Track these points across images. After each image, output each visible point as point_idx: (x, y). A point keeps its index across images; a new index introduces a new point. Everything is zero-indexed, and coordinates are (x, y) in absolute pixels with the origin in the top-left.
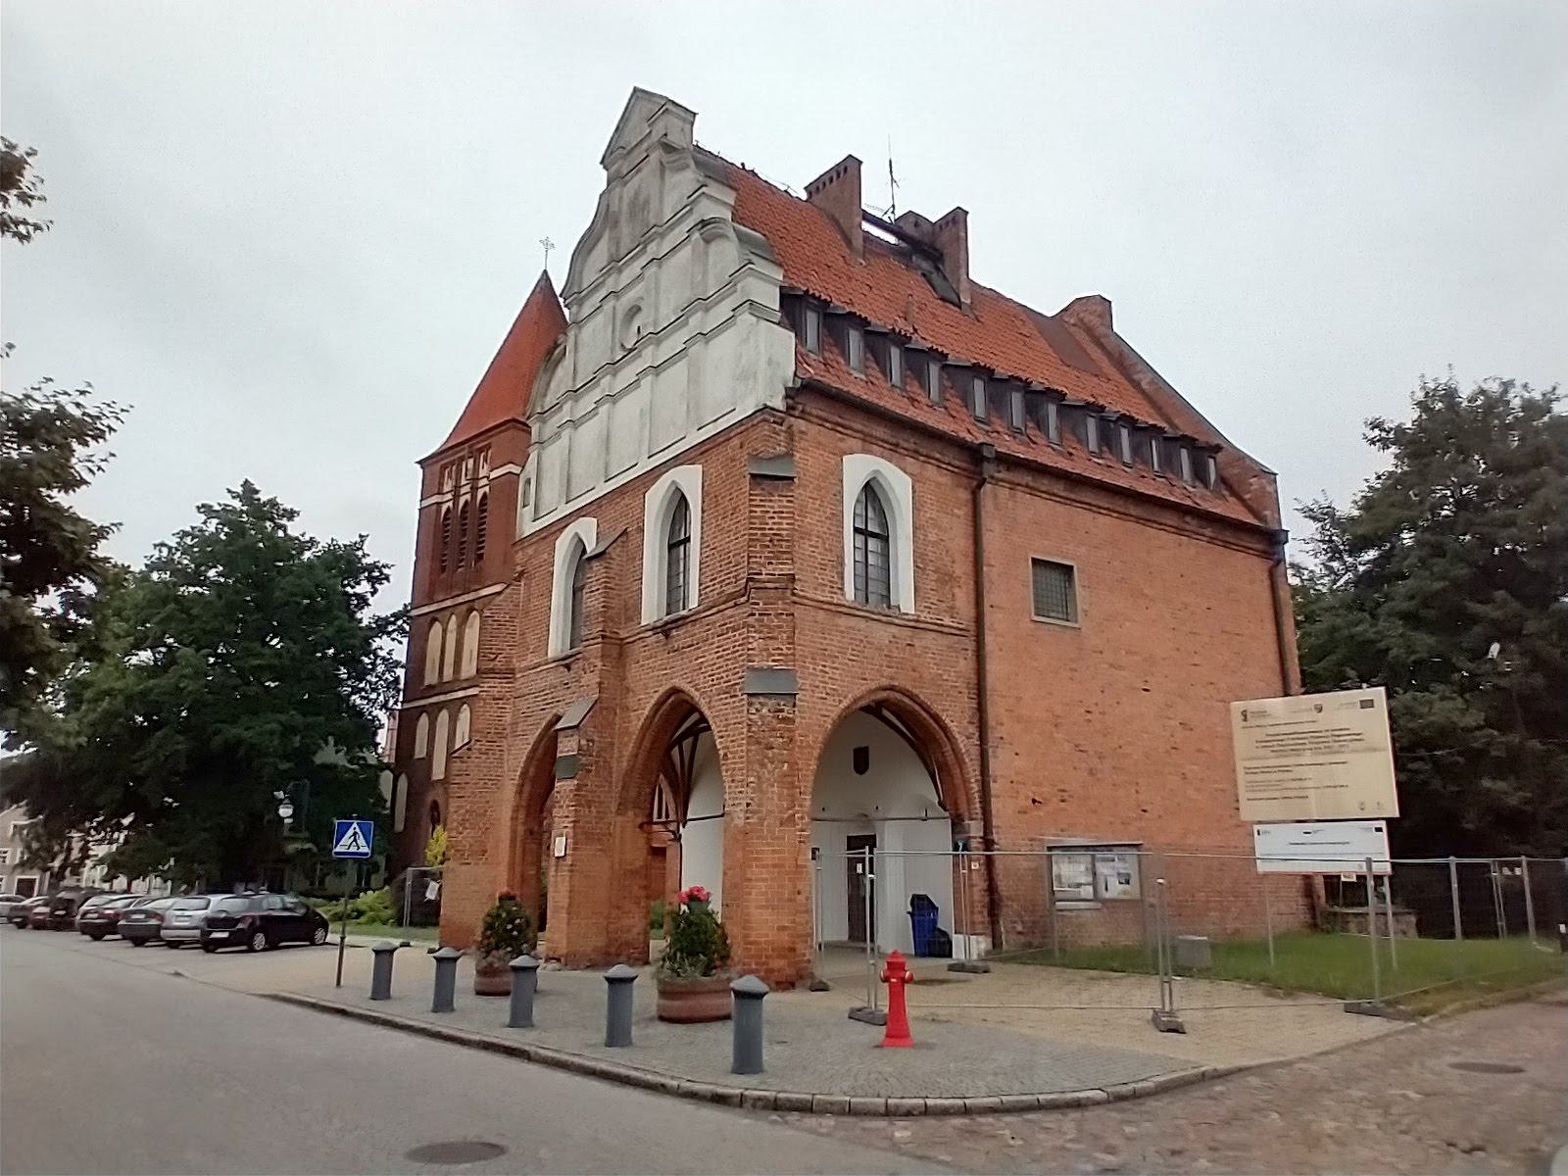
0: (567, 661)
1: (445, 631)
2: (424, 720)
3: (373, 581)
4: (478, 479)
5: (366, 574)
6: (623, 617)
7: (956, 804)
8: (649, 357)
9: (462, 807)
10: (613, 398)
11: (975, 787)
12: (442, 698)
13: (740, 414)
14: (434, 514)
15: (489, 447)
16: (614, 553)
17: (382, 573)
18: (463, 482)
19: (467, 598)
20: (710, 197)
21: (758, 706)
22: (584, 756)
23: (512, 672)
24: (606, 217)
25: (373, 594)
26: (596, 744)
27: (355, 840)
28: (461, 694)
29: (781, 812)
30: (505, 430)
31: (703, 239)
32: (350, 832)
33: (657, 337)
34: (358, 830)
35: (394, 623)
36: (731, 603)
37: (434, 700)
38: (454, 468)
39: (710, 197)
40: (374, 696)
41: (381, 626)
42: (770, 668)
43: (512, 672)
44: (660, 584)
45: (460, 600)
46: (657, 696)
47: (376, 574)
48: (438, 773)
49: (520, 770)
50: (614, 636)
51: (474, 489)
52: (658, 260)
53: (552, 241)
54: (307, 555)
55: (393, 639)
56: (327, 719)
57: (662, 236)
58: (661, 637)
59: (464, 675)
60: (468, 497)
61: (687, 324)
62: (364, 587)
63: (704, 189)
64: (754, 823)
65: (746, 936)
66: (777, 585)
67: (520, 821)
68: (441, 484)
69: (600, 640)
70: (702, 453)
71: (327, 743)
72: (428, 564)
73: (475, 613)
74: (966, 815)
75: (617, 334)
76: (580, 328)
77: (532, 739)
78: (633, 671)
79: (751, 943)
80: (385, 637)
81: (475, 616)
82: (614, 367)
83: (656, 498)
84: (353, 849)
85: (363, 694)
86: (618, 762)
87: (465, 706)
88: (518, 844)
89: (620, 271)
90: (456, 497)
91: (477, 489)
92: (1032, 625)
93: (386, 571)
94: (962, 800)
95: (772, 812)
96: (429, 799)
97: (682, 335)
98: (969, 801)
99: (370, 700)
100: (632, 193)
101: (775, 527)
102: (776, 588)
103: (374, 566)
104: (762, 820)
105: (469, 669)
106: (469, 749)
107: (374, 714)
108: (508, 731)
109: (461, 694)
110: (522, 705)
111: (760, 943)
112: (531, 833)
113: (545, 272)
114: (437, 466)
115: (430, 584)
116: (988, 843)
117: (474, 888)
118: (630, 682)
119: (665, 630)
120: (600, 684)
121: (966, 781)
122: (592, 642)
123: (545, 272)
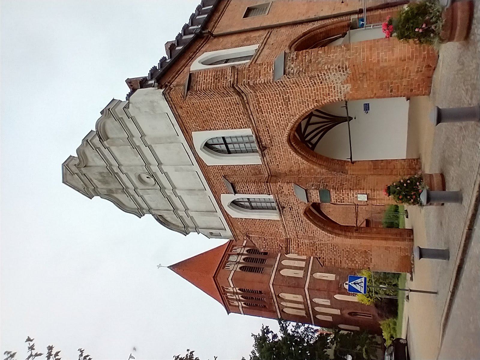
0: (281, 209)
1: (286, 307)
2: (318, 317)
3: (268, 332)
4: (234, 292)
5: (266, 334)
6: (259, 176)
7: (343, 27)
8: (155, 168)
9: (345, 262)
10: (174, 188)
11: (335, 20)
12: (310, 309)
13: (220, 215)
14: (246, 309)
15: (223, 287)
16: (232, 180)
17: (266, 329)
18: (235, 298)
19: (274, 298)
20: (92, 139)
21: (290, 69)
22: (319, 187)
23: (287, 239)
24: (109, 196)
25: (273, 333)
26: (314, 183)
27: (358, 284)
28: (309, 302)
29: (343, 51)
30: (217, 281)
31: (107, 140)
32: (354, 286)
33: (147, 164)
34: (353, 282)
35: (283, 324)
36: (247, 105)
37: (311, 312)
38: (230, 301)
39: (92, 139)
40: (310, 337)
41: (284, 329)
42: (273, 72)
43: (287, 239)
44: (243, 156)
45: (275, 300)
46: (292, 153)
47: (265, 331)
48: (337, 312)
49: (328, 234)
50: (267, 178)
51: (237, 293)
52: (119, 165)
53: (159, 265)
54: (257, 355)
55: (289, 325)
56: (317, 351)
57: (111, 165)
58: (266, 152)
59: (302, 300)
60: (240, 296)
61: (139, 146)
62: (270, 336)
63: (88, 141)
64: (349, 63)
65: (409, 58)
66: (236, 73)
67: (352, 235)
68: (236, 306)
69: (268, 184)
70: (187, 132)
71: (326, 351)
72: (263, 312)
73: (280, 295)
74: (349, 22)
75: (150, 188)
76: (151, 208)
77: (315, 228)
78: (283, 168)
79: (413, 56)
80: (288, 328)
81: (281, 295)
82: (162, 189)
83: (234, 213)
84: (363, 285)
85: (309, 340)
86: (323, 174)
87: (313, 300)
88: (362, 235)
89: (127, 188)
90: (240, 300)
91: (237, 292)
92: (269, 14)
93: (265, 327)
94: (342, 24)
95: (343, 56)
96: (347, 316)
97: (143, 147)
98: (342, 21)
99: (311, 338)
100: (100, 183)
101: (211, 78)
102: (237, 74)
103: (263, 332)
104: (347, 59)
105: (300, 298)
106: (320, 258)
107: (316, 337)
108: (312, 241)
109: (309, 302)
110: (301, 234)
111: (412, 51)
112: (357, 230)
113: (168, 267)
114: (230, 308)
115: (270, 312)
116: (361, 11)
117: (382, 256)
118: (287, 169)
119: (263, 149)
120: (287, 183)
121: (333, 23)
122: (269, 189)
123: (168, 267)
